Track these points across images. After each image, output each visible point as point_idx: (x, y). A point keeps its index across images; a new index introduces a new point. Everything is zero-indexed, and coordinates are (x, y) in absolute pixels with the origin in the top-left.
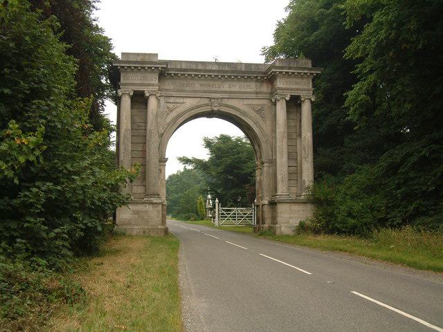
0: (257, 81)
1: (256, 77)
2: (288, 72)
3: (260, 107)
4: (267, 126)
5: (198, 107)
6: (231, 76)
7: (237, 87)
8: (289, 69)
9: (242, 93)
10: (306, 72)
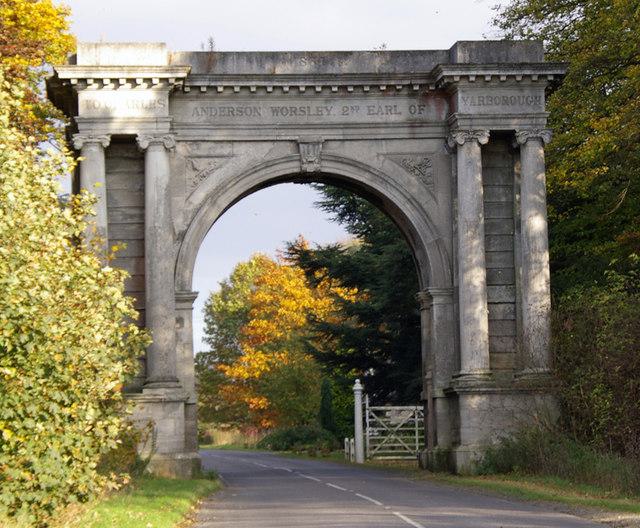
0: (413, 94)
1: (410, 86)
2: (483, 76)
3: (419, 159)
4: (437, 209)
5: (268, 165)
6: (345, 87)
7: (365, 110)
8: (485, 69)
9: (376, 125)
10: (528, 72)
